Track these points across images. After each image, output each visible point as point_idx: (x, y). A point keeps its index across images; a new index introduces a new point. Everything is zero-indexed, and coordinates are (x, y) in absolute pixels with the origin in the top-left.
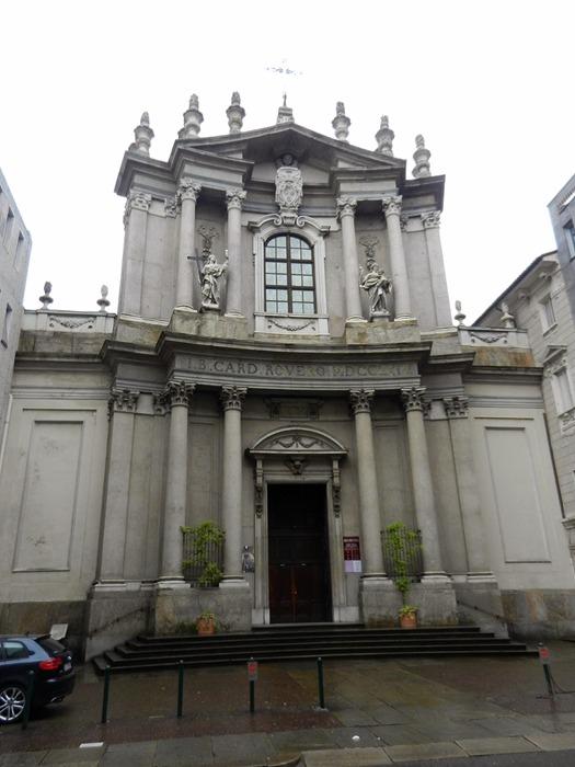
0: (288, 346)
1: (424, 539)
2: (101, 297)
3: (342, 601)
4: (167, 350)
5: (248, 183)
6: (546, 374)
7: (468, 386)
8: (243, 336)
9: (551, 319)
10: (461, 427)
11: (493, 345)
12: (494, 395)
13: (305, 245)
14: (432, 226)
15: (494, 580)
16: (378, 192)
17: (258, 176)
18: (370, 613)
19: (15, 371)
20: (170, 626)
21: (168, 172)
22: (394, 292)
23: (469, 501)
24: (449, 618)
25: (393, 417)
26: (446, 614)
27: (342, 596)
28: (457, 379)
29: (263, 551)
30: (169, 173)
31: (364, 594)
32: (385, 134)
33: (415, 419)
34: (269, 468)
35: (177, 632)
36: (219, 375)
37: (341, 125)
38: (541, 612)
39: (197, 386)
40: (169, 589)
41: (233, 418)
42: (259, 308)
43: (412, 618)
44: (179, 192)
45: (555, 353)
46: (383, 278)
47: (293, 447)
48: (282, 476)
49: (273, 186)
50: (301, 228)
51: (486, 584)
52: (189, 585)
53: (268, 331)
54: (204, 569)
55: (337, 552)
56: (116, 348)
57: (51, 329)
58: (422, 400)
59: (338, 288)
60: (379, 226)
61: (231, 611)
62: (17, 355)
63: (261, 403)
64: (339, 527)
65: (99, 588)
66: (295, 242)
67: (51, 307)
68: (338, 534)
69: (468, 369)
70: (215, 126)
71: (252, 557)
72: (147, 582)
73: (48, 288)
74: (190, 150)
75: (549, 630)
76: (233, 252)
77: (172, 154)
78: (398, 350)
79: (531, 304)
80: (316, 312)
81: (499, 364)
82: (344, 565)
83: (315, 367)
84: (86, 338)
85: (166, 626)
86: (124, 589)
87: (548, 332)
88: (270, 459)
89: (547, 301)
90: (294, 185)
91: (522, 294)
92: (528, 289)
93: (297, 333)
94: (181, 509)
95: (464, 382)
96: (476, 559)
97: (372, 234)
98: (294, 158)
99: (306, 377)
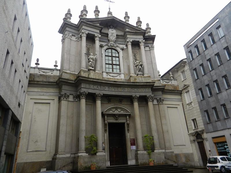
0: (115, 81)
1: (154, 139)
2: (55, 64)
3: (130, 158)
4: (79, 81)
5: (101, 33)
6: (183, 92)
7: (163, 95)
8: (101, 78)
9: (185, 77)
10: (161, 106)
11: (168, 84)
12: (168, 98)
13: (116, 52)
14: (152, 49)
15: (173, 151)
16: (138, 38)
17: (103, 31)
18: (140, 161)
19: (28, 86)
20: (82, 167)
21: (77, 27)
22: (143, 68)
23: (165, 128)
24: (163, 162)
25: (143, 103)
26: (162, 161)
27: (130, 156)
28: (160, 93)
29: (107, 142)
30: (77, 28)
31: (139, 156)
32: (139, 22)
33: (150, 104)
34: (109, 118)
35: (85, 169)
36: (94, 90)
37: (127, 18)
38: (184, 160)
39: (88, 93)
40: (82, 156)
41: (99, 103)
42: (104, 70)
43: (153, 162)
44: (81, 34)
45: (186, 86)
46: (141, 63)
47: (115, 112)
48: (112, 120)
49: (108, 34)
50: (115, 47)
51: (171, 152)
52: (88, 154)
53: (107, 77)
54: (92, 150)
55: (129, 143)
56: (63, 80)
57: (39, 73)
58: (152, 98)
59: (126, 65)
60: (137, 48)
61: (100, 162)
62: (29, 81)
63: (107, 98)
64: (129, 136)
65: (58, 156)
66: (114, 51)
67: (39, 66)
68: (129, 138)
69: (163, 90)
70: (91, 15)
71: (104, 145)
72: (72, 154)
73: (38, 60)
74: (84, 21)
75: (186, 165)
76: (97, 53)
77: (79, 22)
78: (146, 84)
79: (178, 73)
80: (120, 72)
81: (170, 89)
82: (130, 148)
83: (122, 88)
84: (51, 77)
85: (81, 167)
86: (66, 156)
87: (183, 81)
88: (109, 115)
89: (183, 72)
90: (114, 34)
91: (176, 70)
92: (177, 68)
93: (115, 78)
94: (84, 130)
95: (162, 94)
96: (167, 145)
97: (136, 50)
98: (113, 26)
99: (119, 91)
